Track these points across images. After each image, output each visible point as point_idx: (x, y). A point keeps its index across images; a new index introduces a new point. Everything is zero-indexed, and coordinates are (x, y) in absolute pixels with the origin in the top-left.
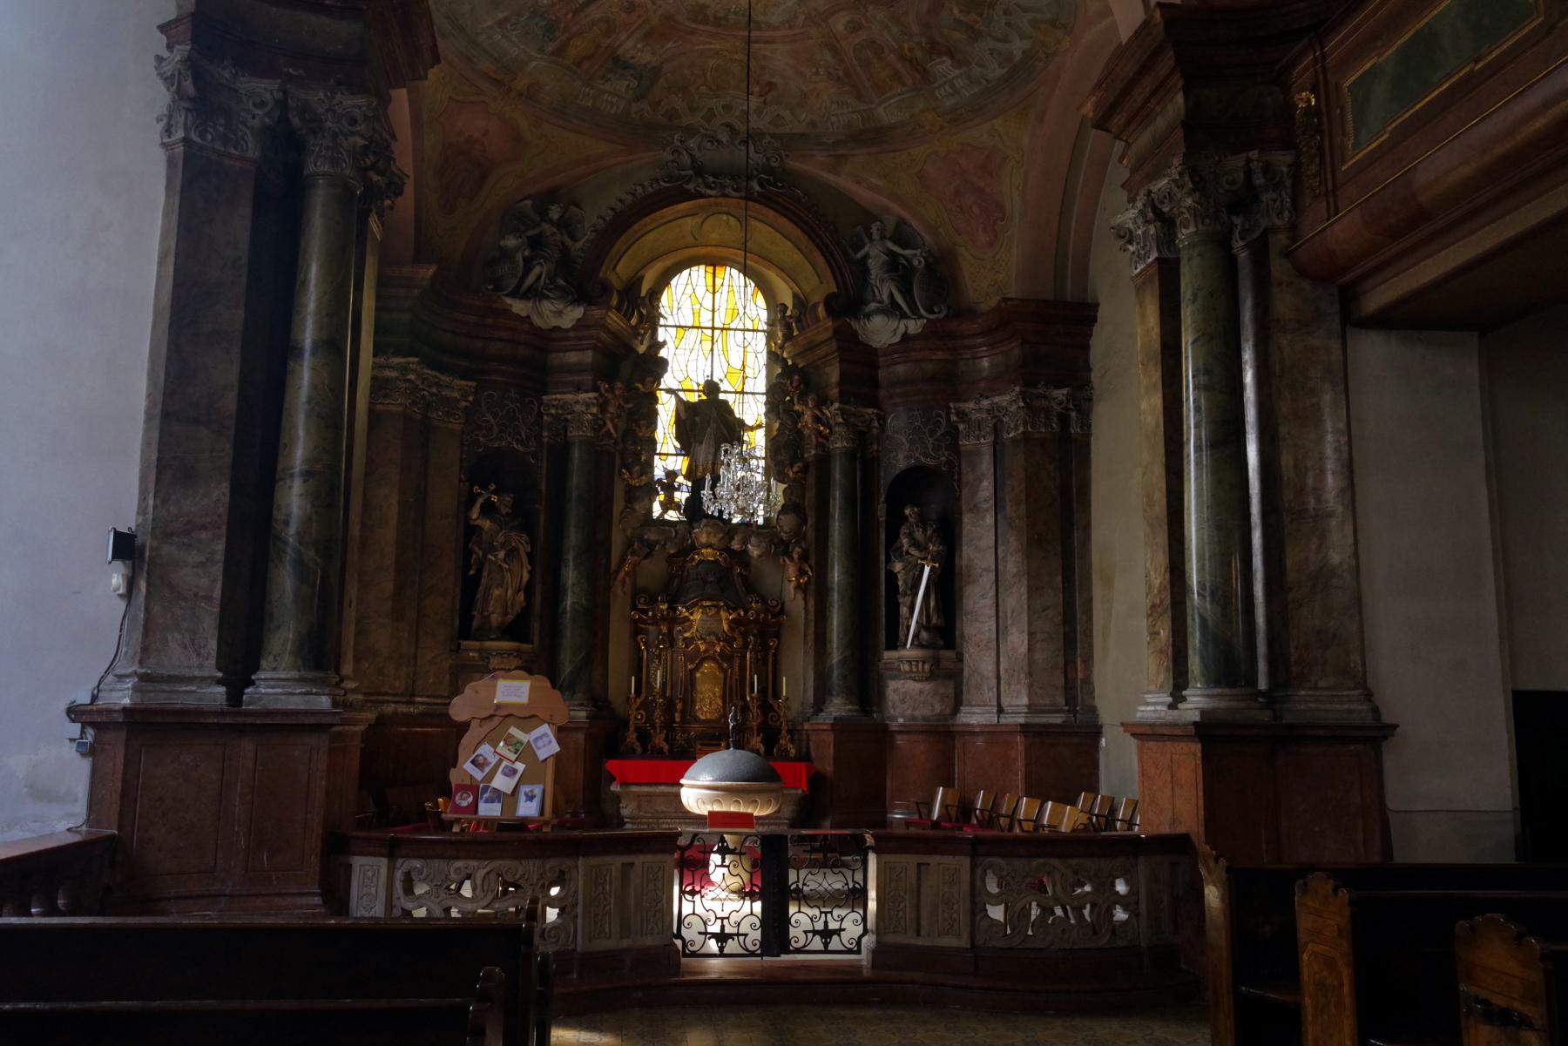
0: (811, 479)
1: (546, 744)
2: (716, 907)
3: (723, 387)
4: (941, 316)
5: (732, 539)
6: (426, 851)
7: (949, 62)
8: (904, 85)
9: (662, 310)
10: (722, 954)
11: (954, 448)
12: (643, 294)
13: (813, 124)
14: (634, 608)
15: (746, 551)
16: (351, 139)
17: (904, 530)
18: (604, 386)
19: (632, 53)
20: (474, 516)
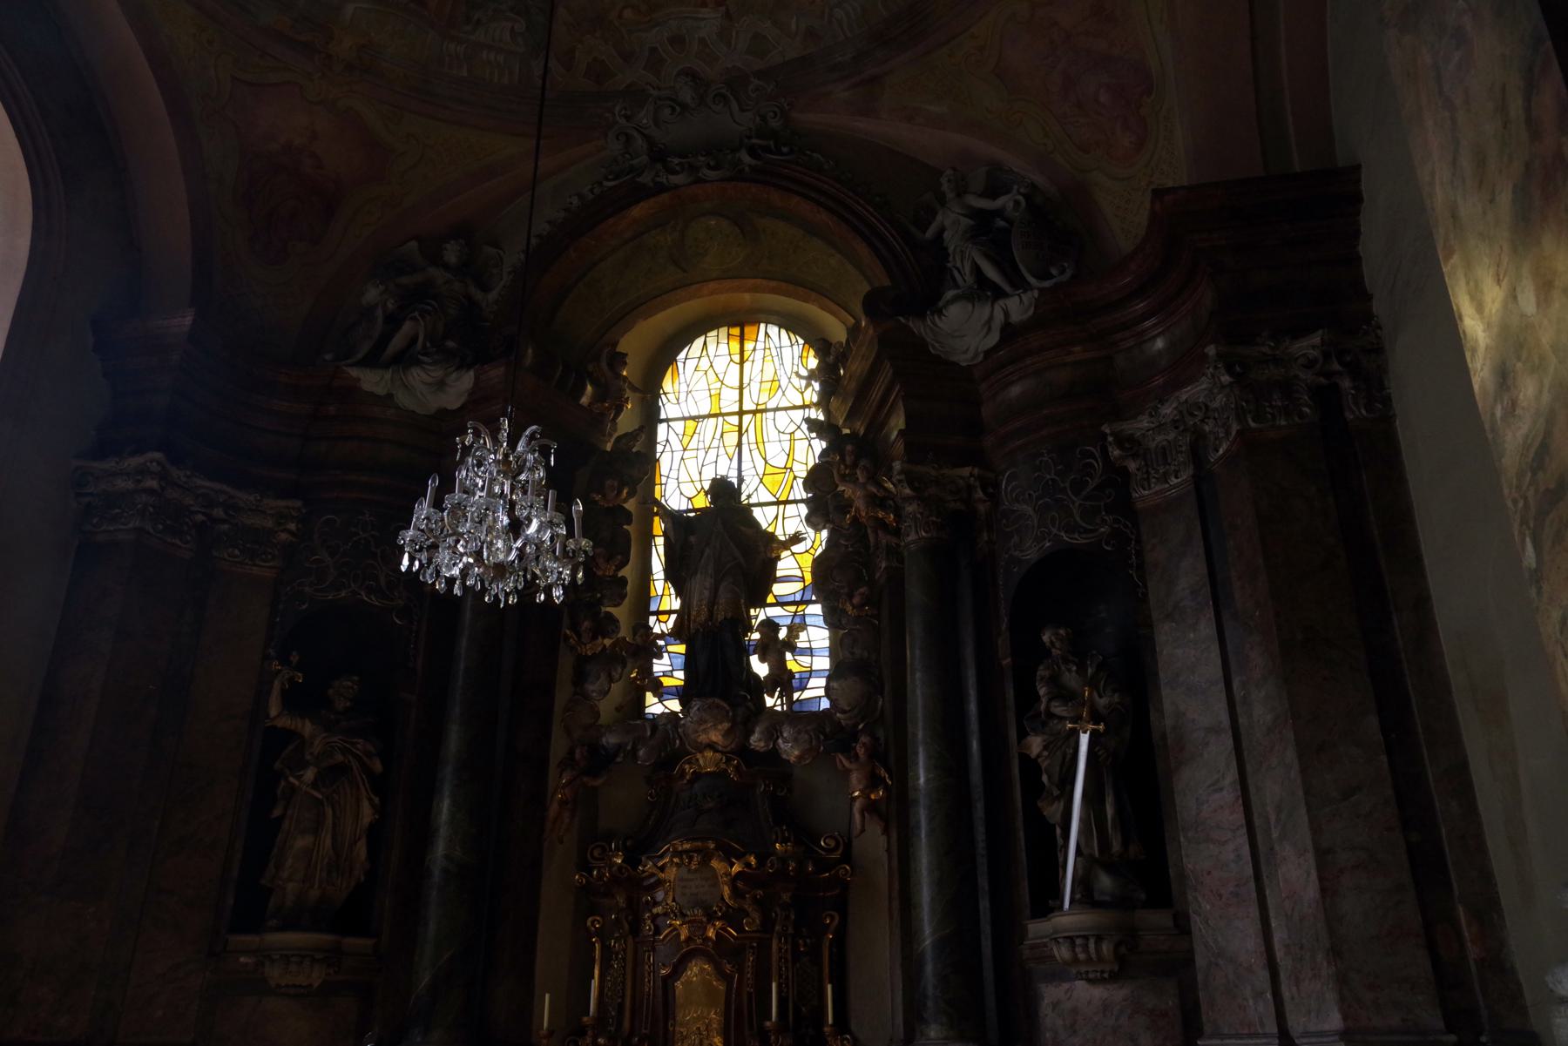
17: (1042, 672)
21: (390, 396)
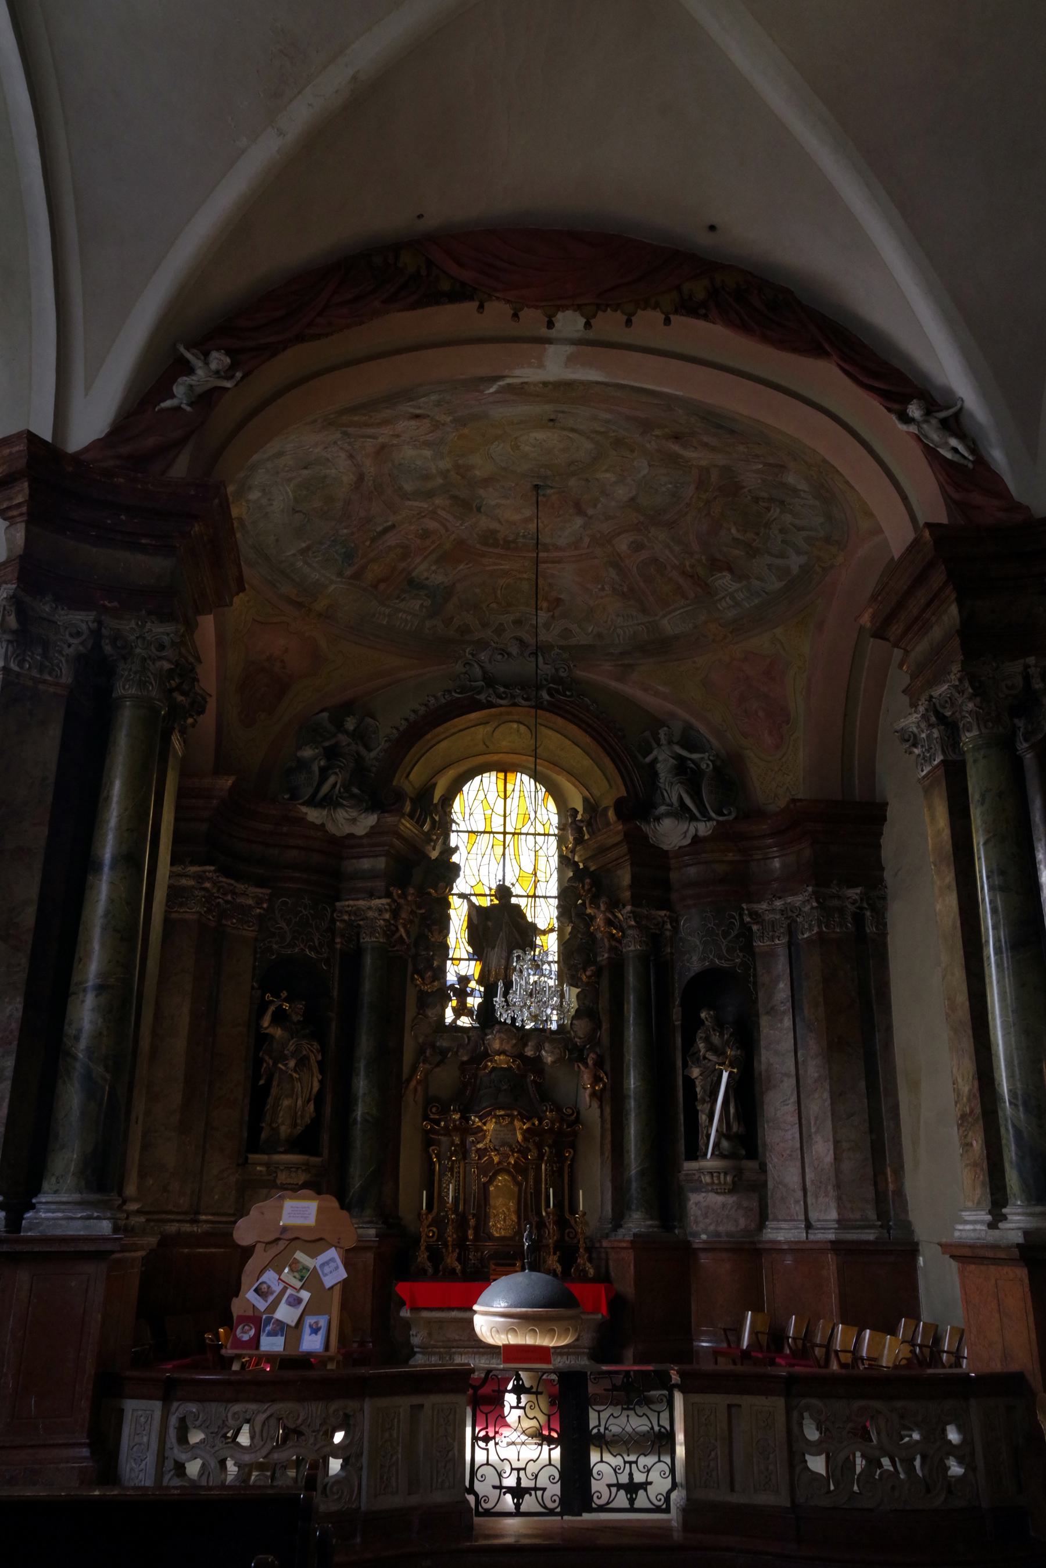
0: (605, 983)
1: (332, 1268)
2: (512, 1451)
3: (514, 891)
4: (731, 818)
5: (525, 1045)
6: (203, 1393)
7: (728, 576)
9: (454, 816)
10: (518, 1513)
11: (749, 949)
12: (435, 801)
14: (426, 1117)
15: (539, 1059)
16: (158, 664)
17: (700, 1034)
18: (396, 892)
19: (426, 574)
20: (266, 1024)
21: (323, 825)
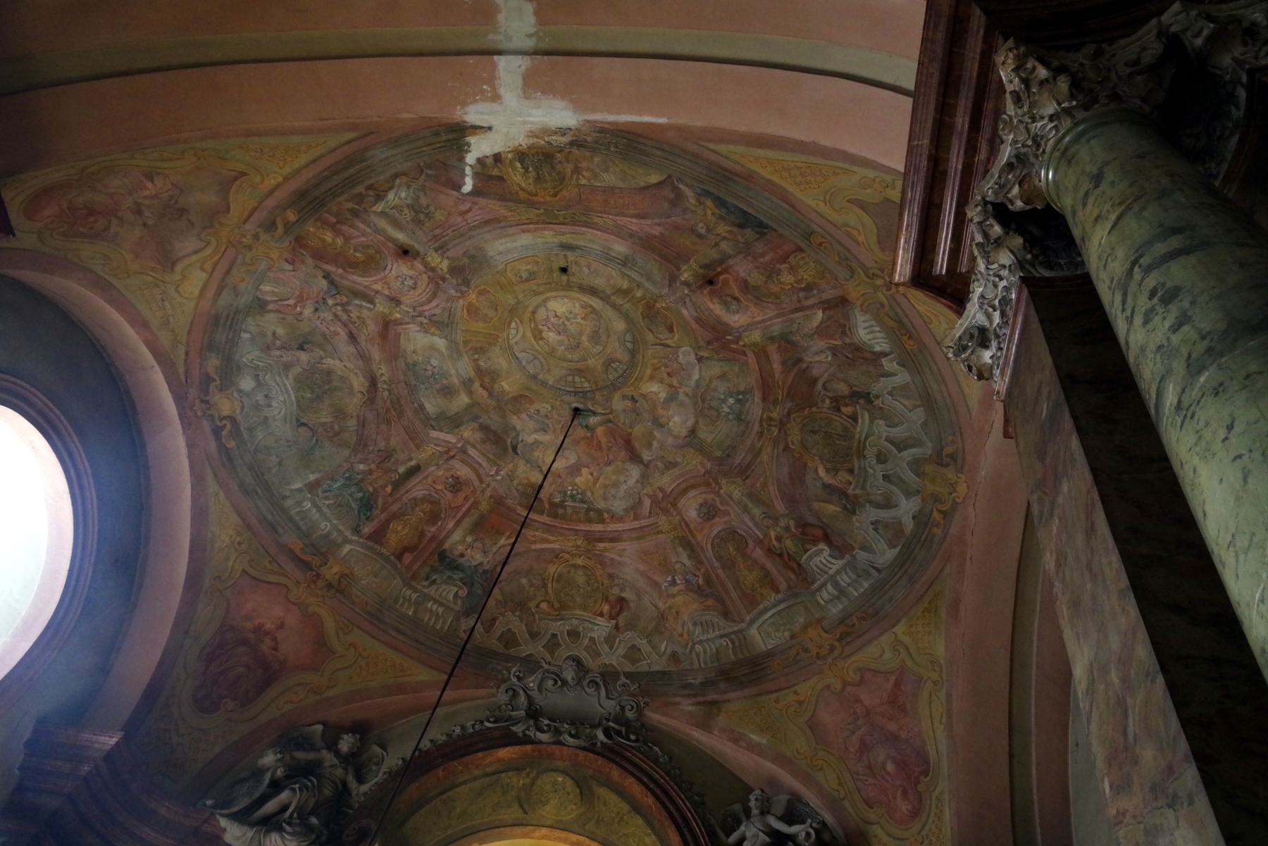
8: (777, 591)
13: (674, 657)
19: (460, 548)
